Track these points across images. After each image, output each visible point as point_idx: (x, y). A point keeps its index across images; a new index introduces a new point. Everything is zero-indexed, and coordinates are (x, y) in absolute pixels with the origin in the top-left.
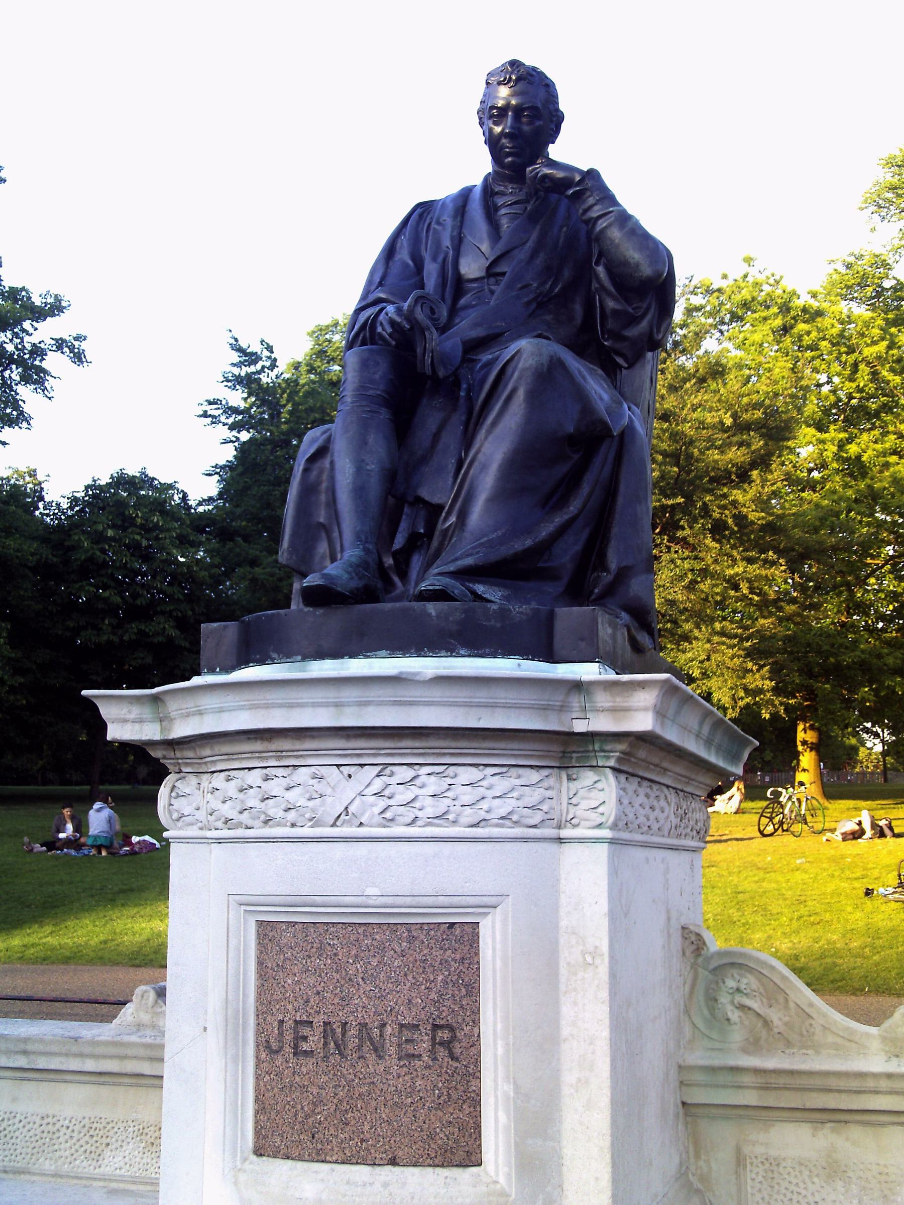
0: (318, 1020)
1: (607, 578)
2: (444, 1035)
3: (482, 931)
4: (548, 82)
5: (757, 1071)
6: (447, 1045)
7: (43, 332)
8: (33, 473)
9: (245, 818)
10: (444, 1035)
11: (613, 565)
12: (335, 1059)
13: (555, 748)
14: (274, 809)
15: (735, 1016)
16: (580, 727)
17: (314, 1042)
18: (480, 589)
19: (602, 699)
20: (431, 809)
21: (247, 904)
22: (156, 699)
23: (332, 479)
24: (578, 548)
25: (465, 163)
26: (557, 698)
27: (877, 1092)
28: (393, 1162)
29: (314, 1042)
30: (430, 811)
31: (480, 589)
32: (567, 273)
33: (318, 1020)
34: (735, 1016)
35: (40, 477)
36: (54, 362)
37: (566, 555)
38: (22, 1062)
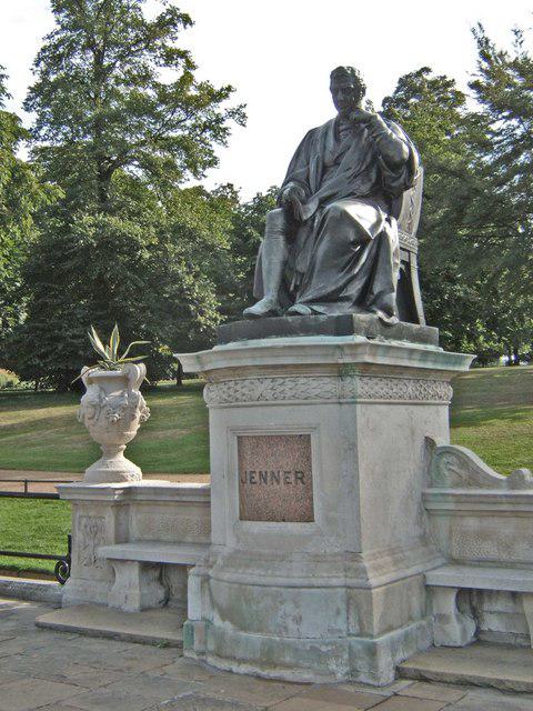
0: (257, 471)
1: (372, 297)
2: (300, 475)
3: (314, 442)
4: (341, 96)
5: (453, 495)
6: (301, 479)
7: (221, 108)
8: (230, 186)
9: (230, 399)
10: (300, 475)
11: (375, 293)
12: (263, 484)
13: (335, 369)
14: (238, 395)
15: (446, 473)
16: (341, 361)
17: (257, 478)
18: (315, 308)
19: (347, 351)
20: (289, 394)
21: (233, 430)
22: (198, 357)
23: (260, 264)
24: (360, 287)
25: (324, 111)
26: (331, 352)
27: (502, 503)
28: (284, 520)
29: (257, 478)
30: (289, 394)
31: (315, 308)
32: (368, 160)
33: (257, 471)
34: (446, 473)
35: (235, 189)
36: (229, 123)
37: (354, 290)
38: (177, 498)
